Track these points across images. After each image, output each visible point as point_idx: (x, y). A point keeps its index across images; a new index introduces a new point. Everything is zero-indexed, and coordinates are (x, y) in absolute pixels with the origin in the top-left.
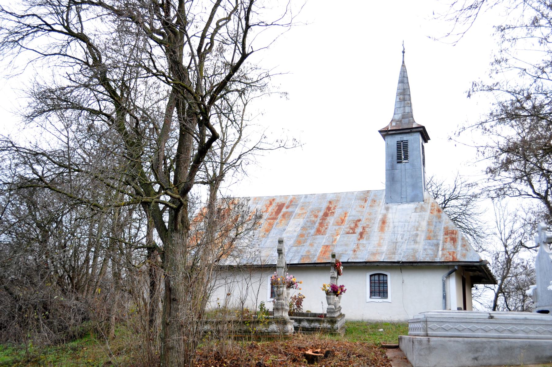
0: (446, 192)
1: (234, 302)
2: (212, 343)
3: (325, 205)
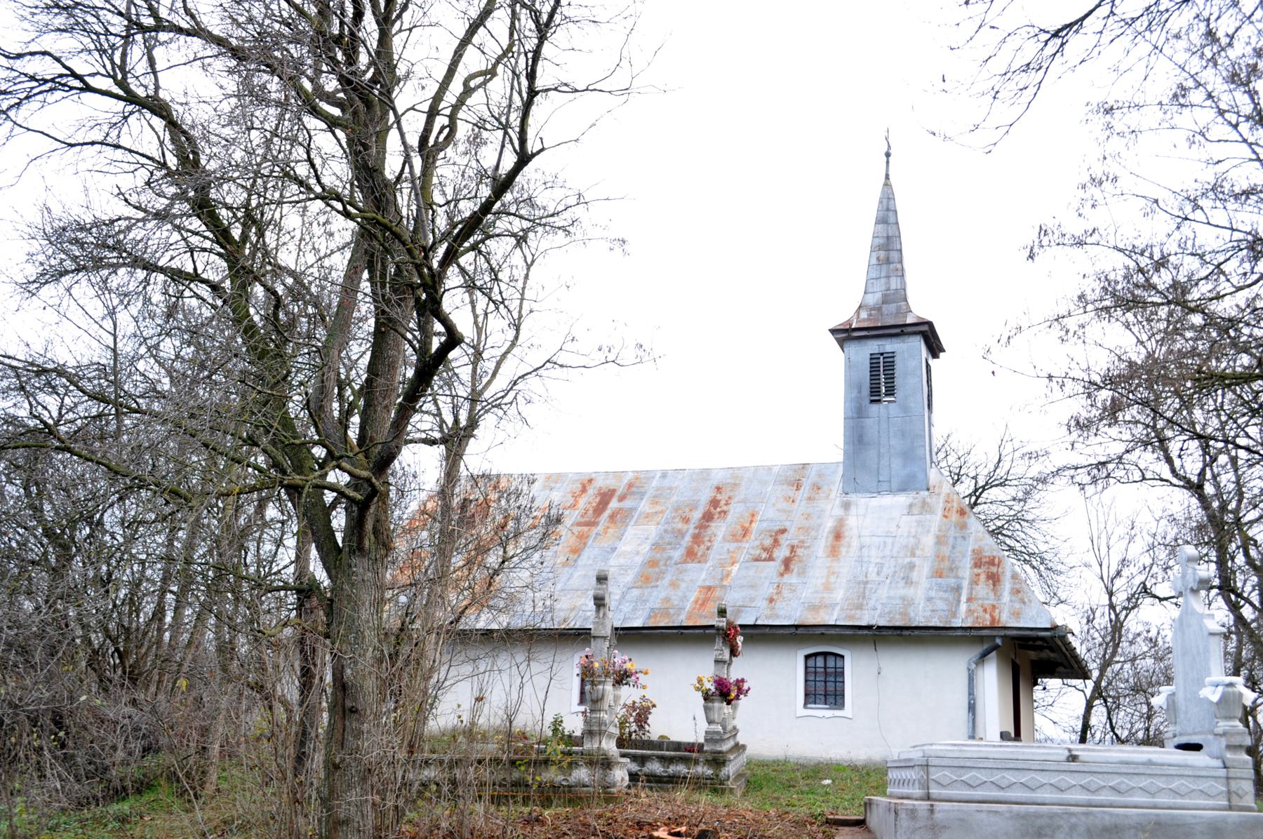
0: (978, 470)
1: (490, 717)
2: (438, 811)
3: (705, 496)
